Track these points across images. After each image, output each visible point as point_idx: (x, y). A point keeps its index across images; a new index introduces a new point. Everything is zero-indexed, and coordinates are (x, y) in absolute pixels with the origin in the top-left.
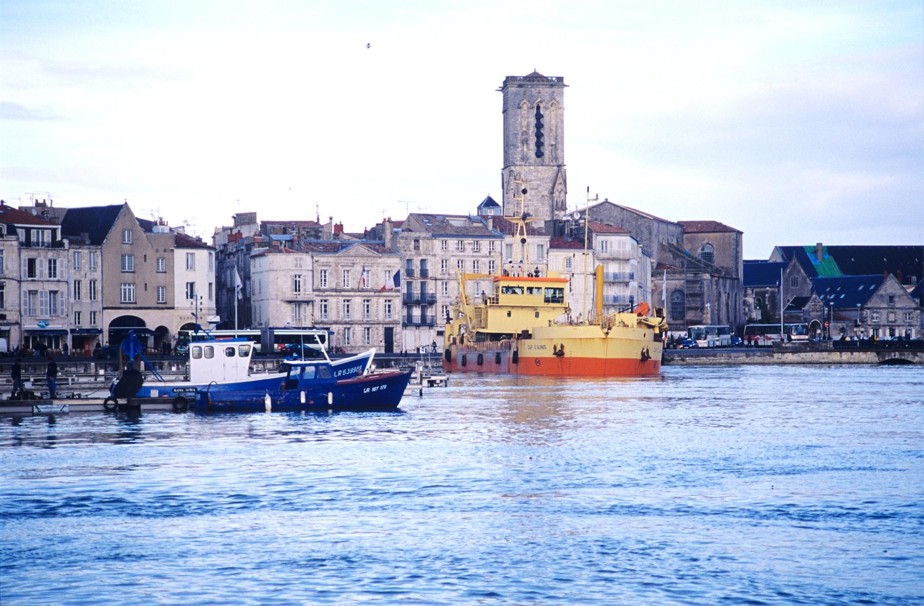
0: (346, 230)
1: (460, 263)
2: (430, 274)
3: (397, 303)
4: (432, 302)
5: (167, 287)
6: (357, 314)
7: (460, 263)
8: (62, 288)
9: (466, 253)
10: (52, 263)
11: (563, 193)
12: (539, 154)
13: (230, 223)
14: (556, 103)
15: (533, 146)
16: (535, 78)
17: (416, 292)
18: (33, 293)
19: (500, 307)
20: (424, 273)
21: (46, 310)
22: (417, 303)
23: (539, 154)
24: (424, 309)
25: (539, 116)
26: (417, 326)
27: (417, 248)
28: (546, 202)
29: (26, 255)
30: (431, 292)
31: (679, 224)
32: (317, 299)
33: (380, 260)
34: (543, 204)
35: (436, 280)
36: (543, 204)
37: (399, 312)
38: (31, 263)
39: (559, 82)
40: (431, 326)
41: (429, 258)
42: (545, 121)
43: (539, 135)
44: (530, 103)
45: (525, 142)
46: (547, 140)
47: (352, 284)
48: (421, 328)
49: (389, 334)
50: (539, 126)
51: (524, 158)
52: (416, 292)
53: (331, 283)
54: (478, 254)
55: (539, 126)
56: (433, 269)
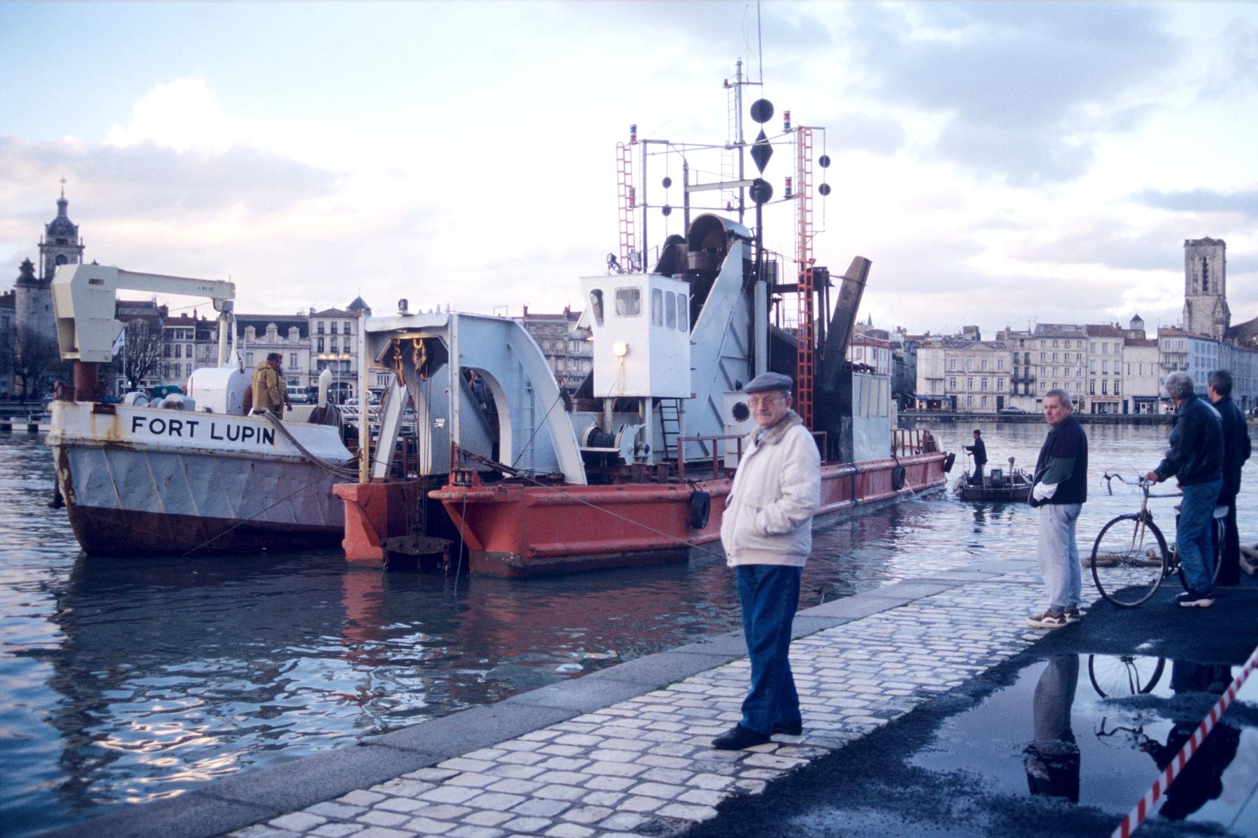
1: (1054, 355)
3: (1007, 381)
4: (1033, 381)
6: (977, 386)
7: (1054, 355)
12: (1205, 289)
13: (307, 313)
16: (1207, 241)
20: (1027, 362)
21: (802, 386)
22: (1022, 381)
23: (1205, 289)
24: (1027, 385)
25: (1205, 265)
26: (1022, 396)
27: (1022, 345)
32: (948, 378)
37: (1007, 386)
40: (1032, 396)
42: (1209, 267)
43: (1205, 277)
47: (973, 368)
50: (1205, 271)
52: (1021, 374)
53: (958, 367)
55: (1205, 271)
56: (1034, 358)
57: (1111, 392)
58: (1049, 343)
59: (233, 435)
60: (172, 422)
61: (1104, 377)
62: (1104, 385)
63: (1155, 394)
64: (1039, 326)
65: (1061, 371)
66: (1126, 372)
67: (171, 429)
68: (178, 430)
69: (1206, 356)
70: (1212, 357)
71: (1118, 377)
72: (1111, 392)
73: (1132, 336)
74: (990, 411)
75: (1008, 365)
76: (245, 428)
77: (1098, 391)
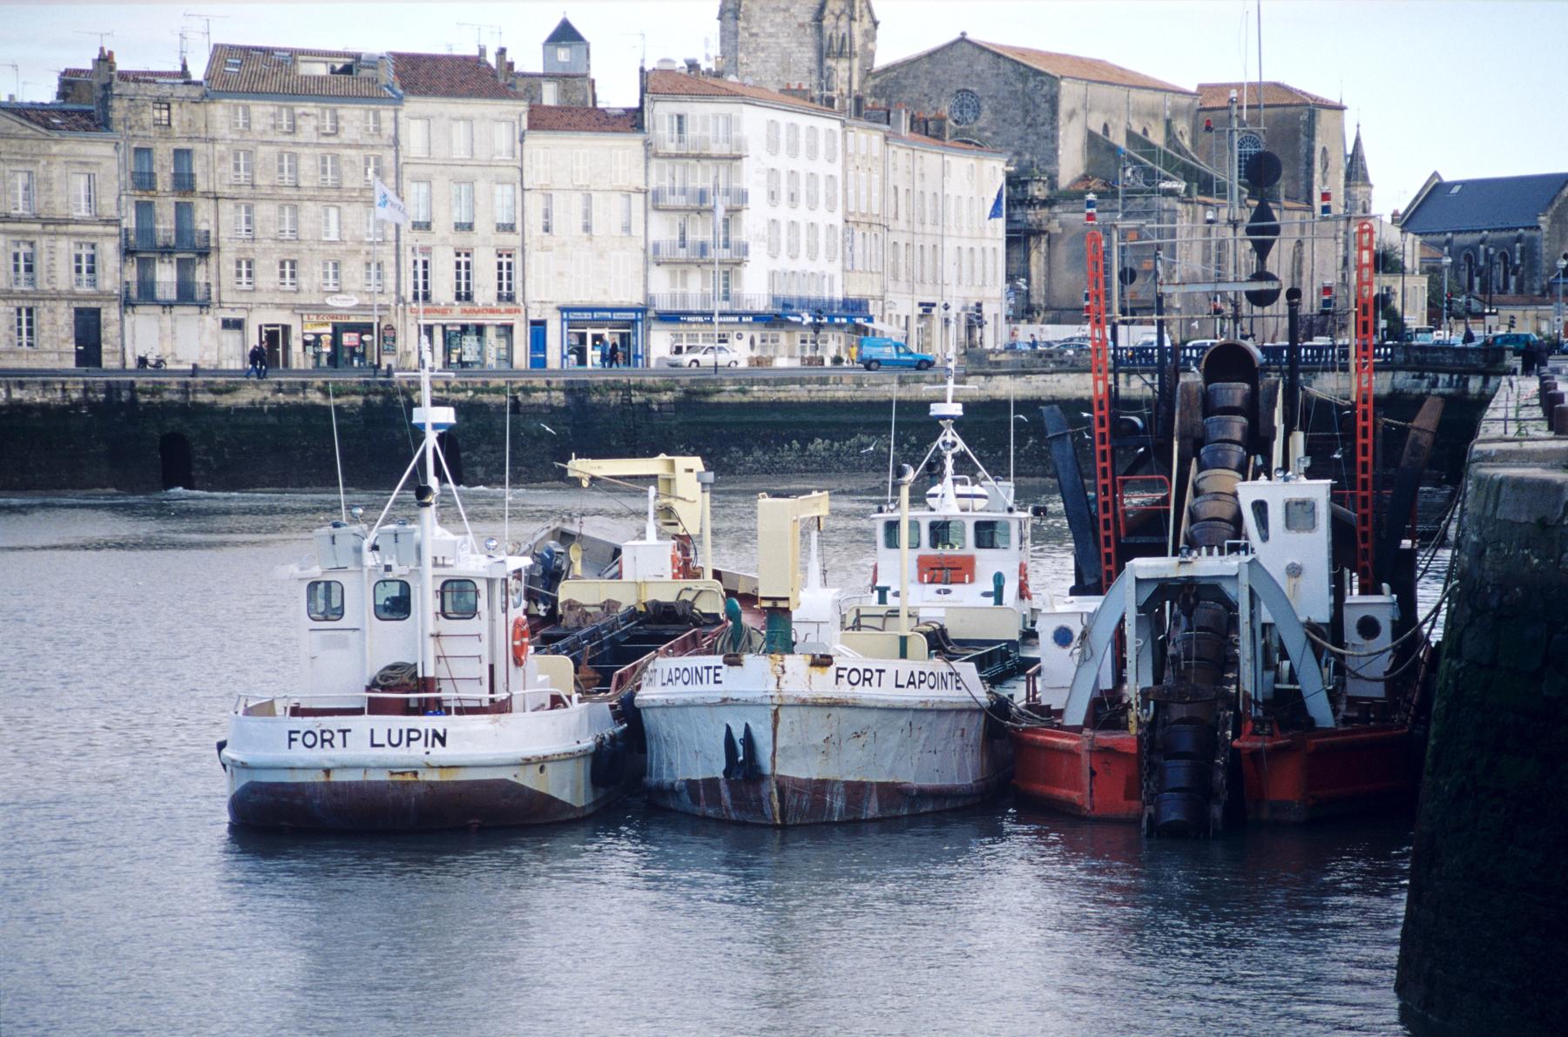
0: (516, 69)
2: (201, 184)
3: (109, 251)
9: (301, 138)
11: (844, 19)
17: (165, 226)
19: (647, 270)
20: (184, 183)
22: (166, 251)
26: (168, 305)
28: (808, 39)
30: (203, 227)
33: (55, 149)
34: (801, 44)
35: (217, 198)
36: (801, 44)
37: (113, 273)
40: (205, 305)
41: (199, 147)
48: (177, 310)
49: (88, 329)
52: (165, 226)
54: (332, 140)
57: (485, 291)
58: (262, 112)
59: (395, 740)
60: (323, 732)
61: (462, 240)
62: (464, 269)
63: (635, 298)
64: (221, 53)
66: (535, 220)
67: (323, 741)
68: (330, 741)
69: (802, 165)
70: (822, 167)
71: (510, 240)
72: (485, 291)
73: (549, 95)
74: (49, 362)
75: (115, 199)
76: (409, 731)
77: (443, 291)
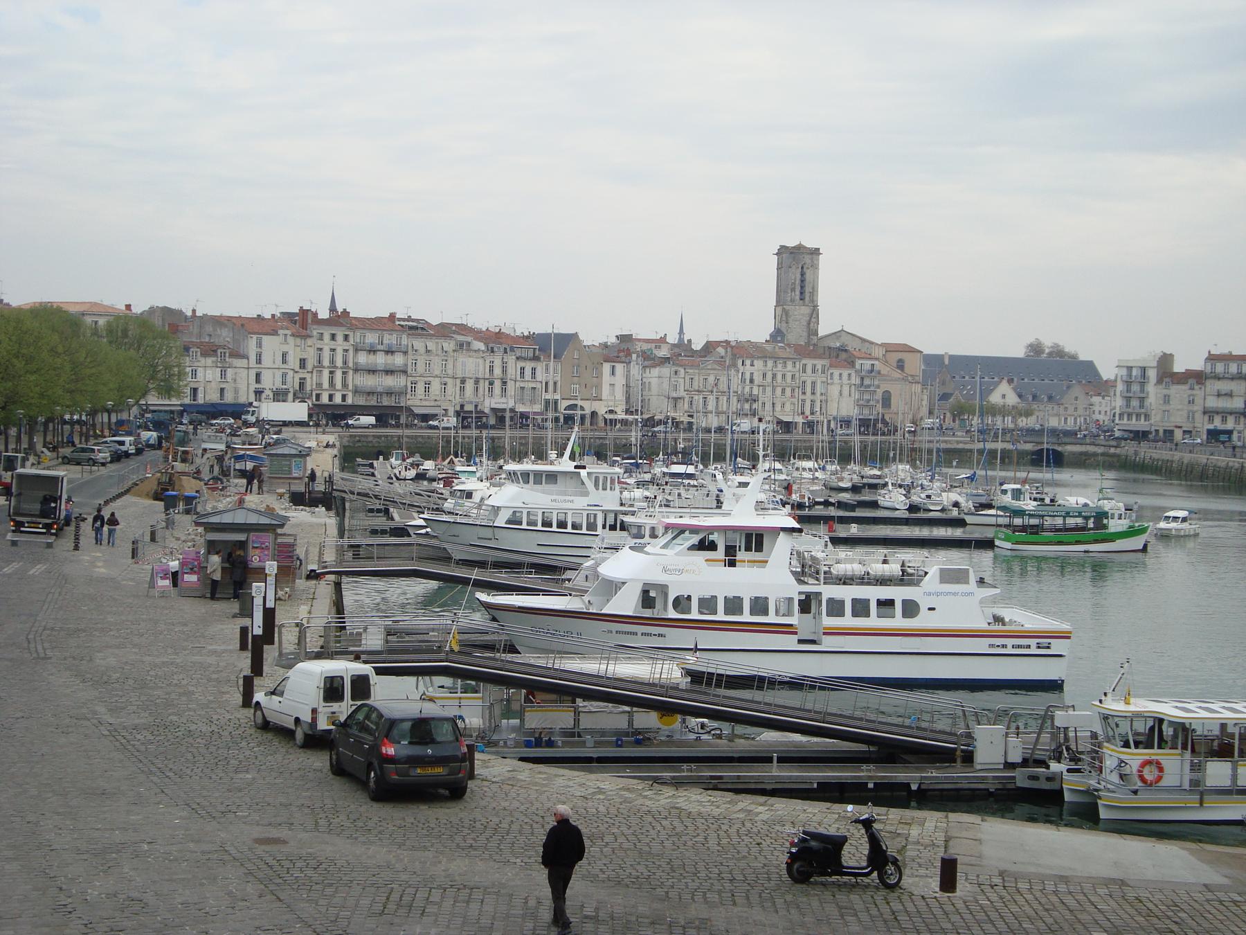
5: (599, 386)
8: (539, 386)
10: (534, 370)
13: (613, 340)
14: (815, 267)
15: (798, 293)
18: (523, 388)
25: (803, 274)
29: (520, 364)
31: (883, 345)
38: (523, 369)
39: (816, 252)
44: (797, 268)
45: (793, 290)
46: (808, 289)
50: (802, 281)
51: (792, 301)
55: (802, 281)
62: (812, 406)
65: (779, 390)
77: (808, 412)
